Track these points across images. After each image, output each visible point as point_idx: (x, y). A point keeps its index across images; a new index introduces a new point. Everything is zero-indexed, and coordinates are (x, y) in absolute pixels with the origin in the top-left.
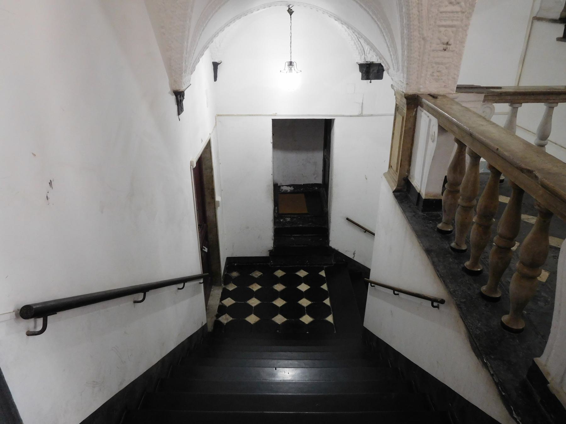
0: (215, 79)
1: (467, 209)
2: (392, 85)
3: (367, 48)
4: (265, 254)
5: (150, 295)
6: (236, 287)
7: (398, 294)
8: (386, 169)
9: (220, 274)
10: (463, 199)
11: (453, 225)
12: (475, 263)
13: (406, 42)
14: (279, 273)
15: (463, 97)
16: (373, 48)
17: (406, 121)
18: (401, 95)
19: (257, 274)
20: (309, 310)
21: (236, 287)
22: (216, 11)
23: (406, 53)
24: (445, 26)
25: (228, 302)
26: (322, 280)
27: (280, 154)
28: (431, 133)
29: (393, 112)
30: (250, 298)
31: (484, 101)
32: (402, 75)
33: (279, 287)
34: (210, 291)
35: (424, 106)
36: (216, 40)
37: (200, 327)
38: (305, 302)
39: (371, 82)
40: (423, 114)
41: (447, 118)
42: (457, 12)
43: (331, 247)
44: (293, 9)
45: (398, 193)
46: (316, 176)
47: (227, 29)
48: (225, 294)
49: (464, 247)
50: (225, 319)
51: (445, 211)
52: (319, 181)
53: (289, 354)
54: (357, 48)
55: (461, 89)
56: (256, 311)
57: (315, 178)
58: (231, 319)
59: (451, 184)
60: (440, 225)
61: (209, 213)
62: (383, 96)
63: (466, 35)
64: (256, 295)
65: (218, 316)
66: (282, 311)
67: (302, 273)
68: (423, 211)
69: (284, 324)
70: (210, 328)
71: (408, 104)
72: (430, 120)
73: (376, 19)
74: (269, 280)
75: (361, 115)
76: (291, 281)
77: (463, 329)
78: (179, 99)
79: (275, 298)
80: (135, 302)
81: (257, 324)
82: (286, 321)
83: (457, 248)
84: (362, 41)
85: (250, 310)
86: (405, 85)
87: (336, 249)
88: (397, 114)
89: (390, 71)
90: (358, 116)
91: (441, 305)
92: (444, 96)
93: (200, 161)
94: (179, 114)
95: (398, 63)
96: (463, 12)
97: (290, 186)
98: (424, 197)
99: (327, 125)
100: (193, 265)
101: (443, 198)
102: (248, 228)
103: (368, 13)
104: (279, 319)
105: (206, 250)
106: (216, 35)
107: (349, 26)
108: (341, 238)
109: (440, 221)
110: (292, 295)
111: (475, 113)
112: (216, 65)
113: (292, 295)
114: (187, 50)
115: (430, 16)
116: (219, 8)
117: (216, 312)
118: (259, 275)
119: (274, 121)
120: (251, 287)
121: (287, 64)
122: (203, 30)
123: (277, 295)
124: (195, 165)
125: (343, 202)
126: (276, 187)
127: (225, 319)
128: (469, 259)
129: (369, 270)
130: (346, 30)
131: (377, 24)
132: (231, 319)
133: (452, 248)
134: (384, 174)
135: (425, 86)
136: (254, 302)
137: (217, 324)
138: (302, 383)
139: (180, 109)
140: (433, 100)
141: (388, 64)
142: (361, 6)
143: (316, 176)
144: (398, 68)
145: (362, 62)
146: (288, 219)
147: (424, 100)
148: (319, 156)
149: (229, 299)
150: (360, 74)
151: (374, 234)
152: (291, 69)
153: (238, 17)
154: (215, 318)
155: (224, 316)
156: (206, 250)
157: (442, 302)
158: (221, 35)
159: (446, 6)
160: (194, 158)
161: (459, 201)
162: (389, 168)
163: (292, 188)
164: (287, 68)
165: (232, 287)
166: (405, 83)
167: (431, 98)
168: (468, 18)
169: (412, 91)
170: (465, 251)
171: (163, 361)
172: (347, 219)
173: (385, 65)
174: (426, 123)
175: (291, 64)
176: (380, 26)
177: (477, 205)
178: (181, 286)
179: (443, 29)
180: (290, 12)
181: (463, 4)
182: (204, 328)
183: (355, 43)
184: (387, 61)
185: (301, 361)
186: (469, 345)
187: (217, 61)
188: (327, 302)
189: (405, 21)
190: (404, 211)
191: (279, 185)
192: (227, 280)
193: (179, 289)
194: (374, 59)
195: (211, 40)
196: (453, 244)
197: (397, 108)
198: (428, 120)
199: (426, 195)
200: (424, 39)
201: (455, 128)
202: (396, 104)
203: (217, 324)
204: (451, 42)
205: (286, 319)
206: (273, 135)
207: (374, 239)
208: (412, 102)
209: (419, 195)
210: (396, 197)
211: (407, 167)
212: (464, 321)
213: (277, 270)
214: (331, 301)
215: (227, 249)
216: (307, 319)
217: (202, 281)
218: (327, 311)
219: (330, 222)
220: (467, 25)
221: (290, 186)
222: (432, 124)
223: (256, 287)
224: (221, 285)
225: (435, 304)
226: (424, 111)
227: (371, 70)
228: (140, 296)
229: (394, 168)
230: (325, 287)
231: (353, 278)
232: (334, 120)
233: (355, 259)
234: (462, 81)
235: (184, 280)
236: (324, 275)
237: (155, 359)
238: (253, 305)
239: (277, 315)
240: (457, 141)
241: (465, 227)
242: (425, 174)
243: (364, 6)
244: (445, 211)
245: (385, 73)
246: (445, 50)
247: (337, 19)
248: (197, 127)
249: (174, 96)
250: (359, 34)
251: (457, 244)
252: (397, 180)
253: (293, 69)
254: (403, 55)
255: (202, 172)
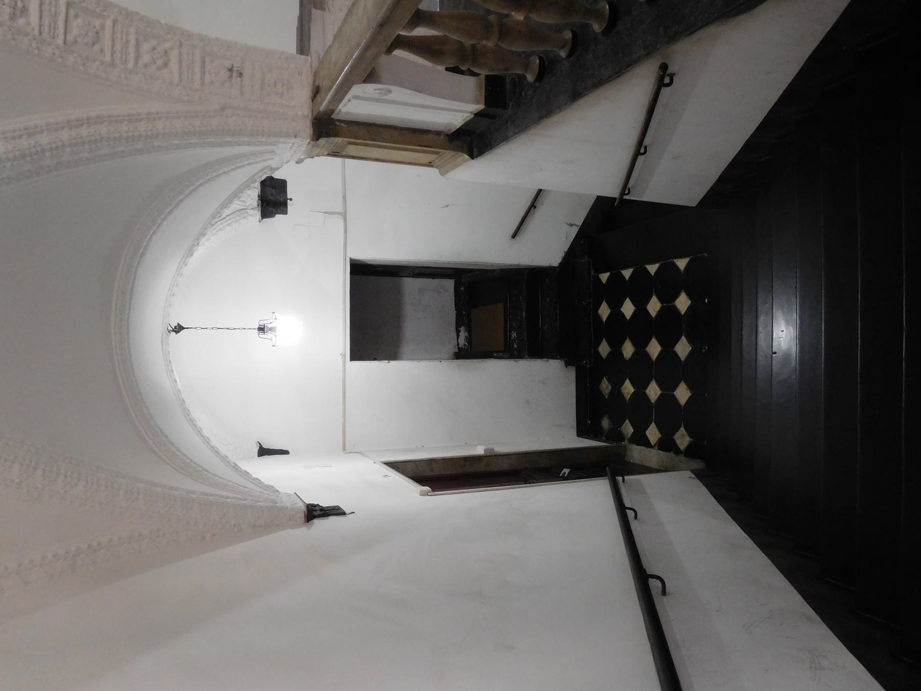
0: (285, 452)
1: (504, 31)
2: (297, 162)
3: (236, 205)
4: (572, 373)
5: (651, 567)
6: (627, 421)
7: (646, 147)
8: (434, 172)
9: (606, 447)
10: (487, 38)
11: (528, 55)
12: (597, 15)
13: (229, 139)
14: (604, 349)
15: (316, 46)
16: (236, 195)
17: (357, 138)
18: (313, 147)
19: (606, 386)
20: (668, 298)
21: (627, 421)
22: (178, 449)
23: (246, 139)
24: (203, 73)
25: (653, 433)
26: (616, 278)
27: (406, 348)
28: (376, 96)
29: (339, 160)
30: (647, 398)
31: (323, 9)
32: (280, 145)
33: (628, 349)
34: (634, 464)
35: (331, 107)
36: (223, 451)
37: (697, 482)
38: (654, 306)
39: (291, 199)
40: (344, 110)
41: (352, 68)
42: (180, 55)
43: (561, 264)
44: (174, 324)
45: (475, 150)
46: (442, 291)
47: (206, 433)
48: (640, 439)
49: (568, 35)
50: (682, 439)
51: (507, 69)
52: (450, 284)
53: (746, 331)
54: (236, 221)
55: (303, 47)
56: (668, 387)
57: (446, 291)
58: (682, 429)
59: (460, 61)
60: (530, 78)
61: (505, 465)
62: (313, 176)
63: (217, 39)
64: (640, 387)
65: (677, 451)
66: (668, 345)
67: (604, 311)
68: (505, 107)
69: (690, 341)
70: (698, 465)
71: (328, 135)
72: (355, 97)
73: (192, 188)
74: (616, 368)
75: (344, 215)
76: (617, 329)
77: (711, 30)
78: (318, 513)
79: (647, 356)
80: (664, 592)
81: (690, 387)
82: (686, 337)
83: (569, 46)
84: (226, 212)
85: (667, 397)
86: (298, 140)
87: (563, 255)
88: (344, 153)
89: (274, 166)
90: (345, 220)
91: (669, 71)
92: (315, 75)
93: (420, 479)
94: (344, 514)
95: (262, 153)
96: (181, 46)
97: (458, 332)
98: (481, 107)
99: (361, 271)
100: (590, 497)
101: (484, 73)
102: (528, 402)
103: (181, 201)
104: (683, 348)
105: (566, 471)
106: (216, 452)
107: (203, 234)
108: (545, 247)
109: (522, 78)
110: (641, 328)
111: (345, 21)
112: (263, 452)
113: (641, 328)
114: (240, 499)
115: (186, 98)
116: (172, 444)
117: (672, 455)
118: (607, 382)
119: (353, 358)
120: (628, 397)
121: (262, 335)
122: (207, 471)
123: (641, 353)
124: (427, 488)
125: (485, 244)
126: (461, 354)
127: (682, 439)
128: (588, 24)
129: (599, 198)
130: (209, 240)
131: (198, 187)
132: (682, 429)
133: (570, 55)
134: (442, 174)
135: (299, 107)
136: (653, 391)
137: (691, 452)
138: (801, 306)
139: (336, 511)
140: (322, 93)
141: (262, 170)
142: (170, 213)
143: (442, 291)
144: (270, 152)
145: (258, 214)
146: (514, 335)
147: (322, 108)
148: (410, 285)
149: (647, 433)
150: (279, 217)
151: (540, 191)
152: (270, 329)
153: (187, 413)
154: (682, 457)
155: (678, 442)
156: (566, 471)
157: (664, 67)
158: (214, 442)
159: (171, 72)
160: (413, 490)
161: (490, 44)
162: (432, 166)
163: (462, 329)
164: (269, 335)
165: (628, 429)
166: (293, 140)
167: (318, 98)
168: (190, 36)
169: (307, 129)
170: (573, 32)
171: (763, 546)
172: (514, 236)
173: (266, 173)
174: (361, 104)
175: (261, 329)
176: (201, 181)
177: (497, 14)
178: (630, 514)
179: (207, 78)
180: (179, 329)
181: (167, 45)
182: (700, 475)
183: (229, 225)
184: (256, 171)
185: (760, 308)
186: (743, 17)
187: (256, 449)
188: (652, 269)
189: (195, 141)
190: (505, 139)
191: (457, 350)
192: (615, 435)
193: (636, 517)
194: (252, 195)
195: (224, 459)
196: (563, 54)
197: (335, 154)
198: (354, 102)
199: (478, 103)
200: (223, 109)
201: (369, 54)
202: (329, 155)
203: (691, 452)
204: (227, 63)
205: (683, 338)
206: (375, 359)
207: (549, 191)
208: (326, 128)
209: (478, 115)
210: (481, 153)
211: (430, 136)
212: (701, 28)
213: (598, 353)
214: (652, 262)
215: (560, 434)
216: (683, 303)
217: (620, 479)
218: (668, 269)
219: (519, 265)
220: (202, 38)
221: (458, 332)
222: (363, 95)
223: (628, 388)
224: (625, 447)
225: (667, 80)
226: (340, 107)
227: (271, 198)
228: (654, 584)
229: (432, 157)
230: (627, 273)
231: (613, 225)
232: (351, 260)
233: (580, 223)
234: (291, 46)
235: (622, 509)
236: (608, 274)
237: (761, 559)
238: (659, 392)
239: (675, 353)
240: (390, 50)
241: (533, 34)
242: (443, 106)
243: (141, 251)
244: (507, 69)
245: (277, 175)
246: (241, 74)
247: (190, 252)
248: (365, 484)
249: (315, 521)
250: (214, 217)
251: (563, 47)
252: (453, 153)
253: (269, 326)
254: (249, 144)
255: (438, 476)
